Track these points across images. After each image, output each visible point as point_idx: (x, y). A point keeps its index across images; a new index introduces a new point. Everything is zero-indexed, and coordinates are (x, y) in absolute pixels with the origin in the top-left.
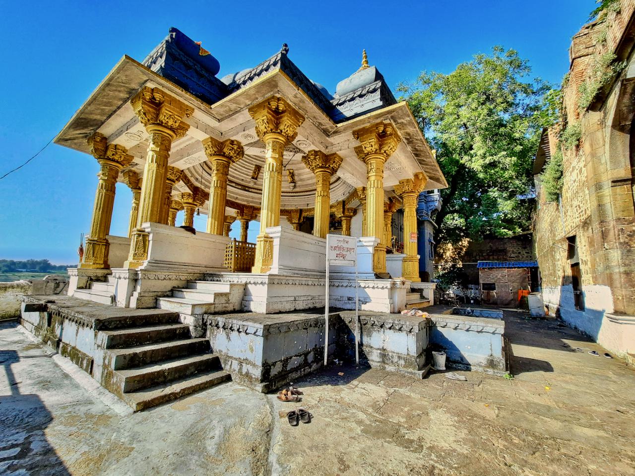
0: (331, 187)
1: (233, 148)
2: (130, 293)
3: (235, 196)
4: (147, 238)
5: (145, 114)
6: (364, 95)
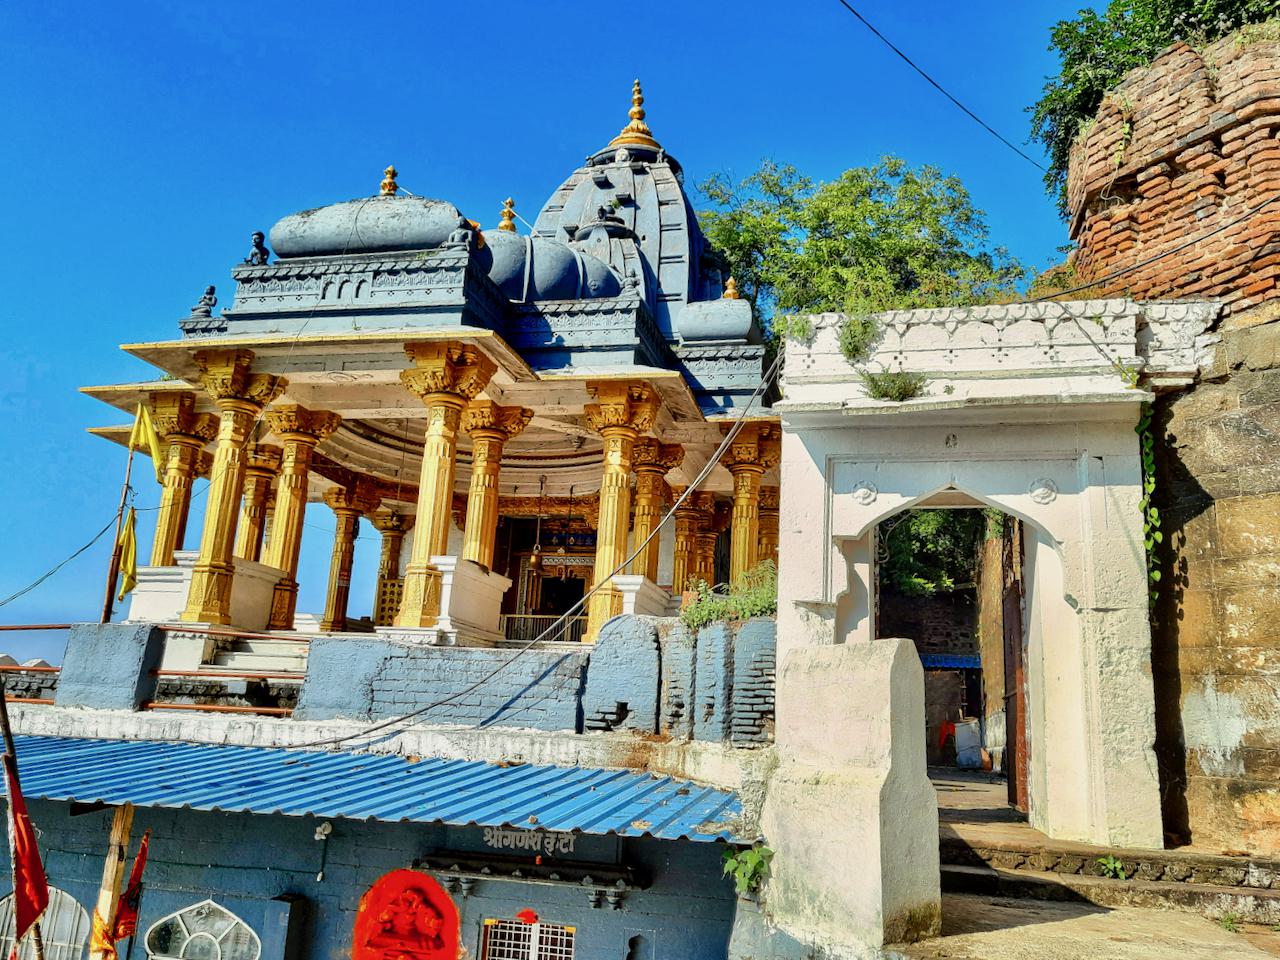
3: (346, 451)
6: (736, 359)
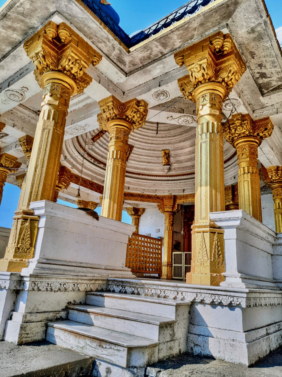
0: (225, 170)
1: (138, 111)
2: (7, 316)
4: (36, 225)
5: (44, 57)
